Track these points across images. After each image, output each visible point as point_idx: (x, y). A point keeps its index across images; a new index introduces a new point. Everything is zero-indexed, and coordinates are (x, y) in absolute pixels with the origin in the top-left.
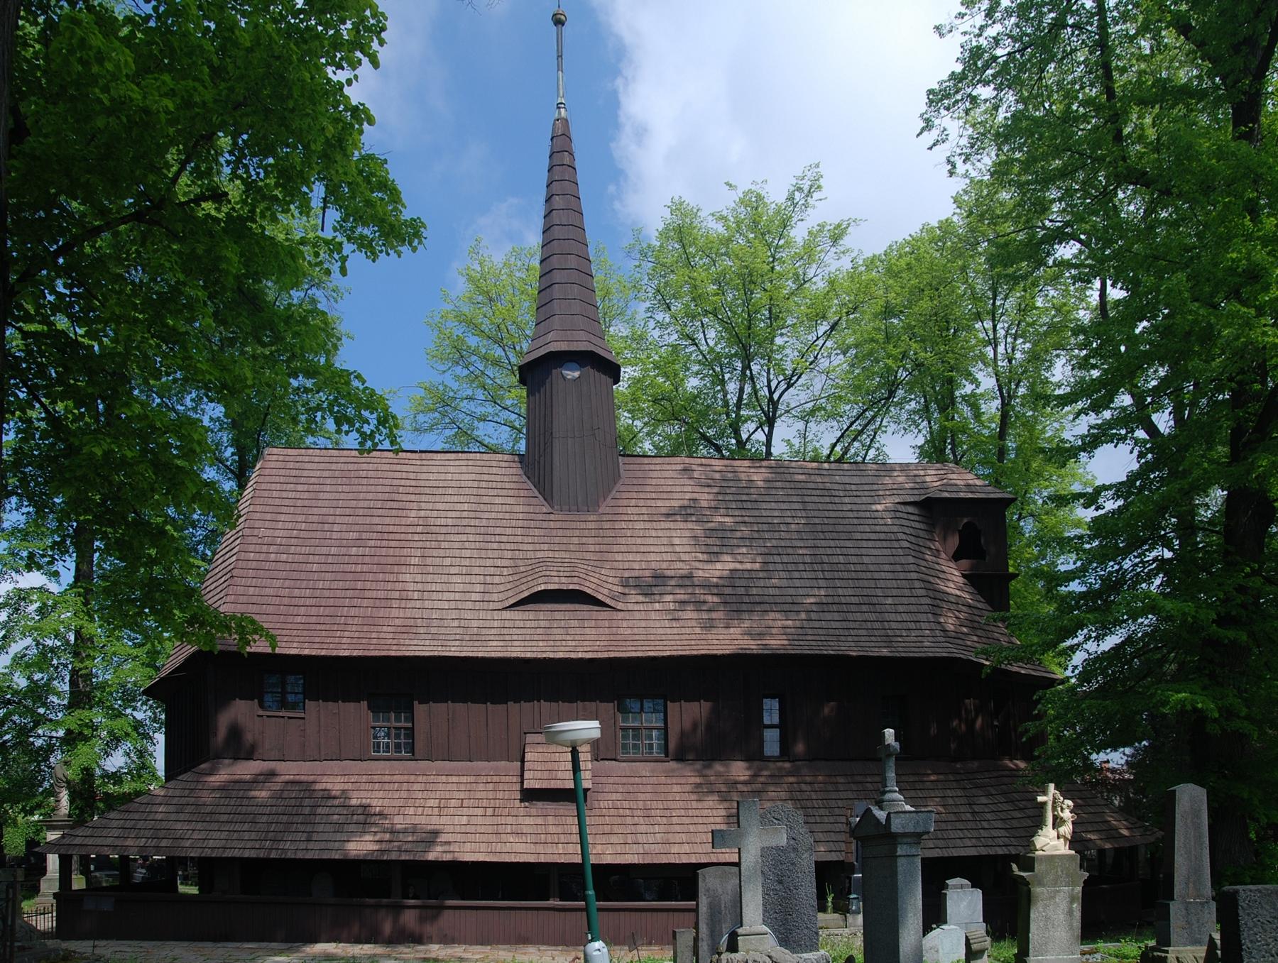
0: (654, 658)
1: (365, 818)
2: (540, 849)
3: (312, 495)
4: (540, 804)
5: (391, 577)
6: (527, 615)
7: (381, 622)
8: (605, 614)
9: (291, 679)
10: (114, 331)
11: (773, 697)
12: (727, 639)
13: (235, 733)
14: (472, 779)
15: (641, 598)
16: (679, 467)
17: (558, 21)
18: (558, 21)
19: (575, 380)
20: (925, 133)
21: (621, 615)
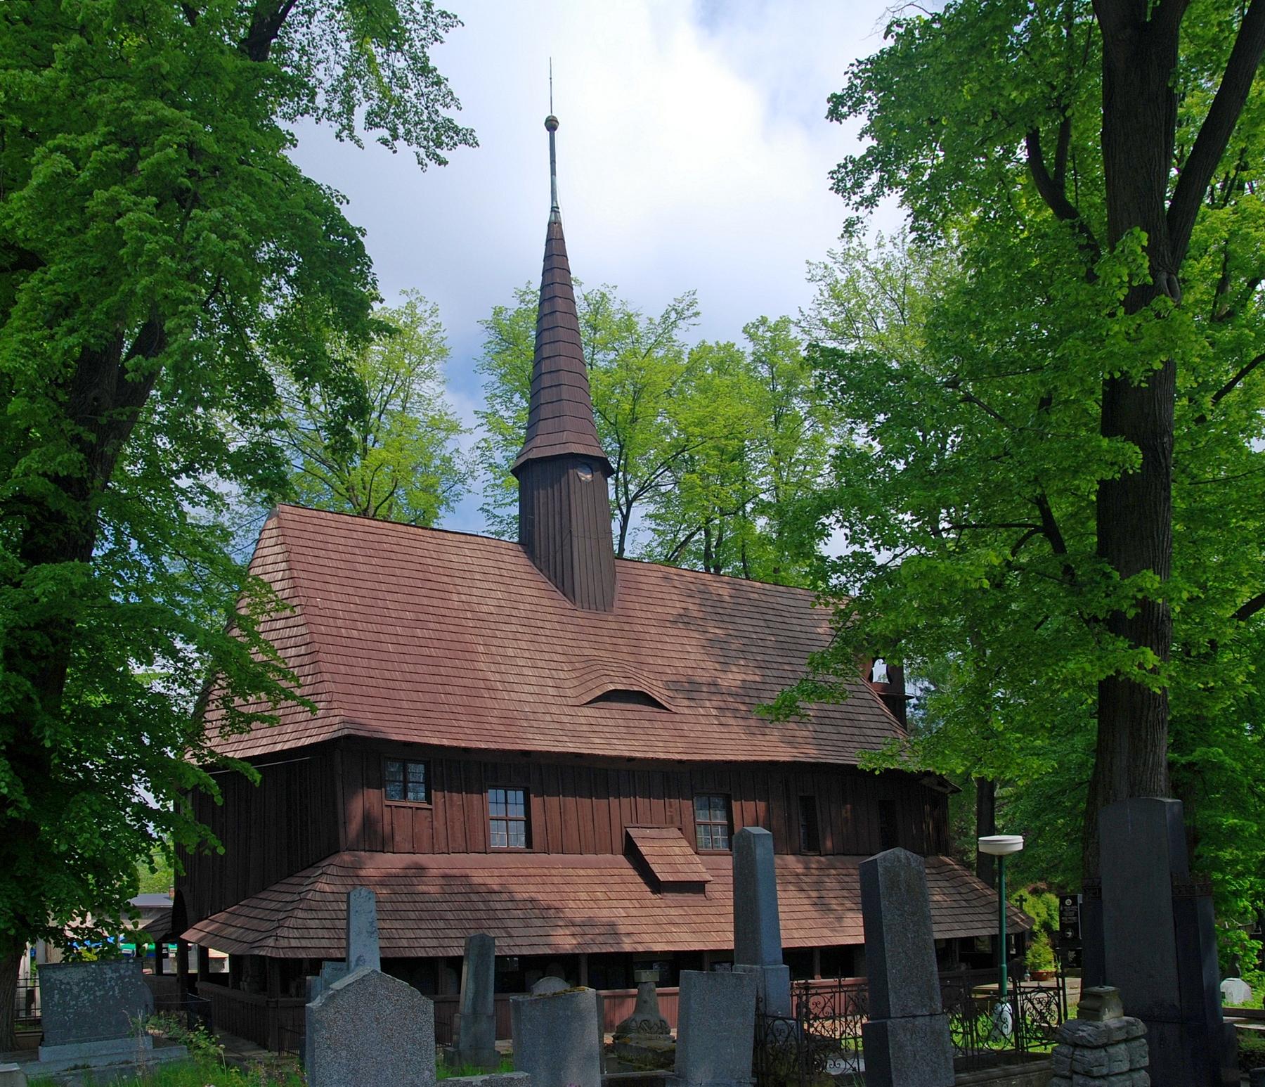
0: (730, 762)
1: (547, 914)
2: (700, 937)
3: (348, 565)
4: (669, 895)
5: (466, 664)
6: (596, 713)
7: (486, 712)
8: (665, 716)
9: (411, 767)
10: (945, 541)
11: (417, 762)
12: (772, 747)
13: (369, 822)
14: (597, 872)
15: (686, 703)
16: (660, 575)
17: (551, 125)
18: (551, 125)
19: (587, 483)
20: (546, 216)
21: (677, 718)
